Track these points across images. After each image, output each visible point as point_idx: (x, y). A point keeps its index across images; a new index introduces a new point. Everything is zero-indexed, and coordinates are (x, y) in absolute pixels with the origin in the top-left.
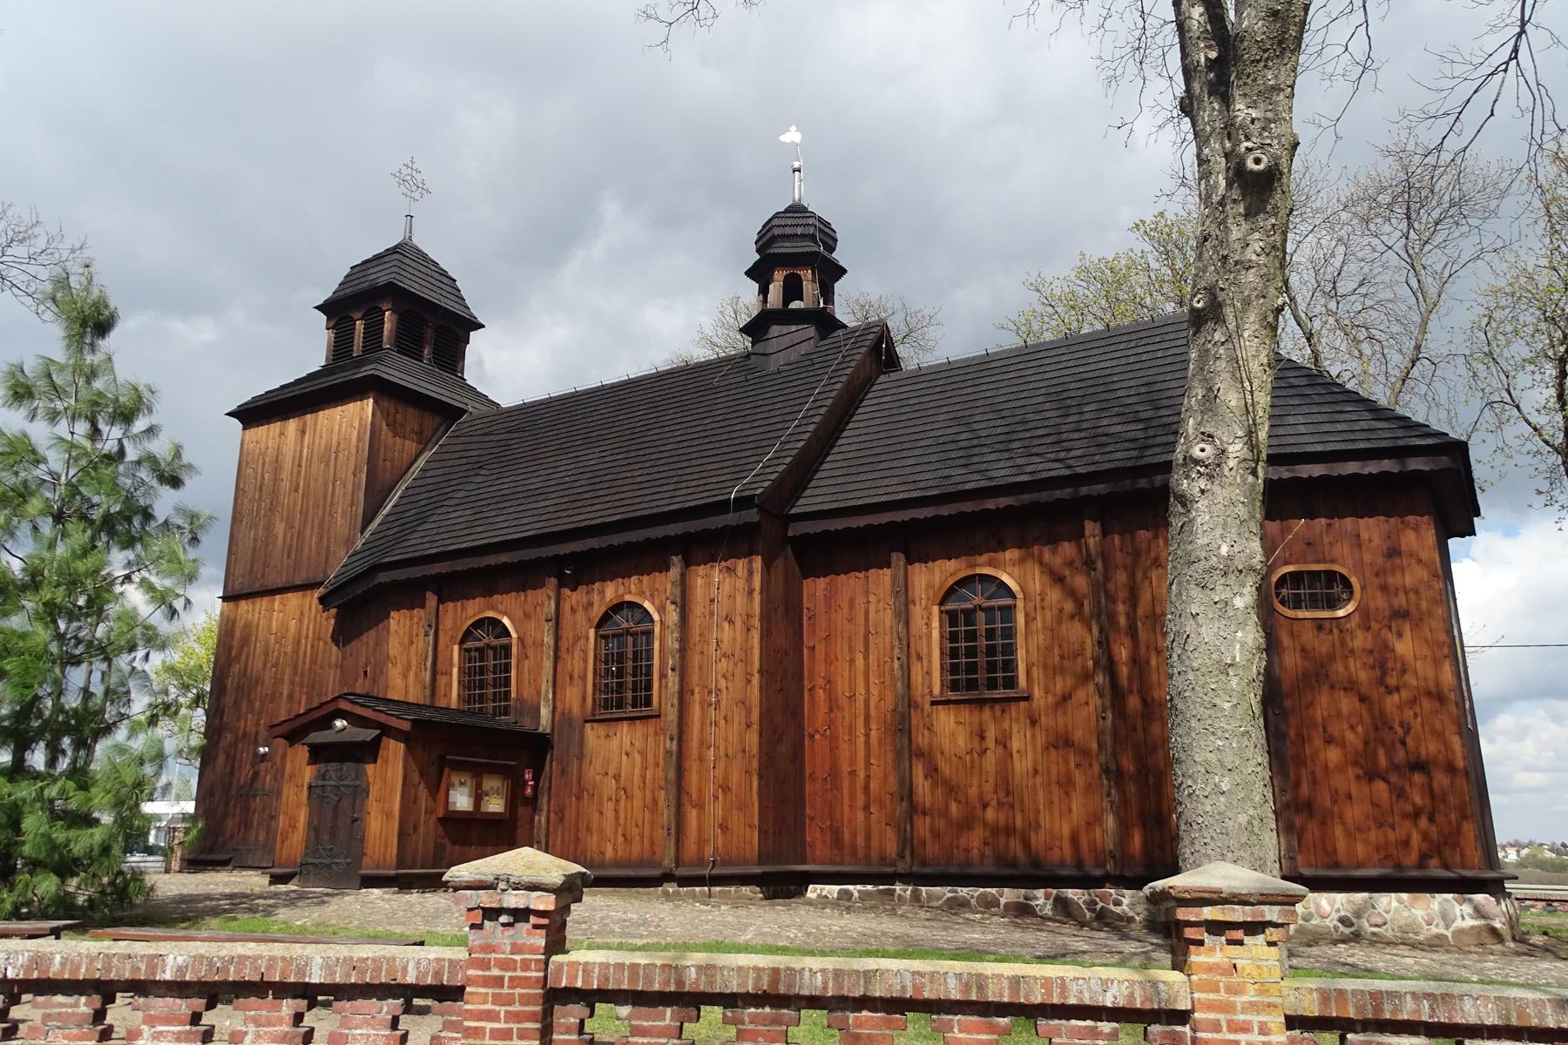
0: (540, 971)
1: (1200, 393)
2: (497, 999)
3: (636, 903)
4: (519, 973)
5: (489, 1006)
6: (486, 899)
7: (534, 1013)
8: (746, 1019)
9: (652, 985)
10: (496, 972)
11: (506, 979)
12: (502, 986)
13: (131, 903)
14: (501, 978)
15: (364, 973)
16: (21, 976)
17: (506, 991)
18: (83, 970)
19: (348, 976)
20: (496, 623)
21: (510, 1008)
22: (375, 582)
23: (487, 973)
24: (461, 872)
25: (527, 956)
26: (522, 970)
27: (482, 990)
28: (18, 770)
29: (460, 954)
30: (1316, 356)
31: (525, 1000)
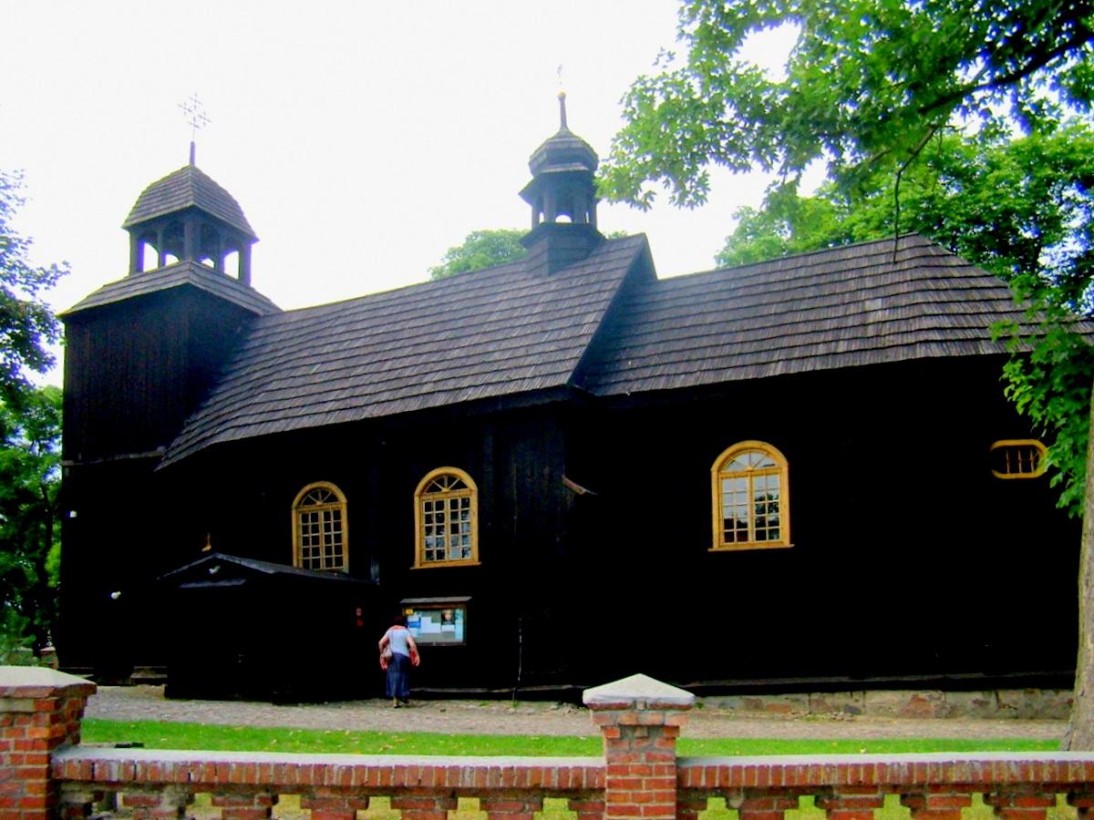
0: (672, 774)
1: (934, 123)
2: (635, 798)
3: (356, 708)
4: (654, 777)
5: (630, 804)
6: (625, 718)
7: (669, 808)
8: (841, 804)
9: (793, 782)
10: (633, 777)
11: (644, 782)
12: (640, 787)
13: (925, 809)
14: (639, 781)
15: (511, 779)
16: (203, 780)
17: (644, 791)
18: (258, 776)
19: (498, 781)
20: (325, 492)
21: (650, 805)
22: (212, 443)
23: (626, 778)
24: (589, 695)
25: (661, 763)
26: (657, 774)
27: (623, 791)
28: (824, 6)
29: (600, 761)
30: (590, 334)
31: (662, 797)
